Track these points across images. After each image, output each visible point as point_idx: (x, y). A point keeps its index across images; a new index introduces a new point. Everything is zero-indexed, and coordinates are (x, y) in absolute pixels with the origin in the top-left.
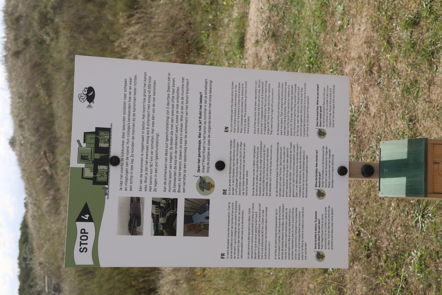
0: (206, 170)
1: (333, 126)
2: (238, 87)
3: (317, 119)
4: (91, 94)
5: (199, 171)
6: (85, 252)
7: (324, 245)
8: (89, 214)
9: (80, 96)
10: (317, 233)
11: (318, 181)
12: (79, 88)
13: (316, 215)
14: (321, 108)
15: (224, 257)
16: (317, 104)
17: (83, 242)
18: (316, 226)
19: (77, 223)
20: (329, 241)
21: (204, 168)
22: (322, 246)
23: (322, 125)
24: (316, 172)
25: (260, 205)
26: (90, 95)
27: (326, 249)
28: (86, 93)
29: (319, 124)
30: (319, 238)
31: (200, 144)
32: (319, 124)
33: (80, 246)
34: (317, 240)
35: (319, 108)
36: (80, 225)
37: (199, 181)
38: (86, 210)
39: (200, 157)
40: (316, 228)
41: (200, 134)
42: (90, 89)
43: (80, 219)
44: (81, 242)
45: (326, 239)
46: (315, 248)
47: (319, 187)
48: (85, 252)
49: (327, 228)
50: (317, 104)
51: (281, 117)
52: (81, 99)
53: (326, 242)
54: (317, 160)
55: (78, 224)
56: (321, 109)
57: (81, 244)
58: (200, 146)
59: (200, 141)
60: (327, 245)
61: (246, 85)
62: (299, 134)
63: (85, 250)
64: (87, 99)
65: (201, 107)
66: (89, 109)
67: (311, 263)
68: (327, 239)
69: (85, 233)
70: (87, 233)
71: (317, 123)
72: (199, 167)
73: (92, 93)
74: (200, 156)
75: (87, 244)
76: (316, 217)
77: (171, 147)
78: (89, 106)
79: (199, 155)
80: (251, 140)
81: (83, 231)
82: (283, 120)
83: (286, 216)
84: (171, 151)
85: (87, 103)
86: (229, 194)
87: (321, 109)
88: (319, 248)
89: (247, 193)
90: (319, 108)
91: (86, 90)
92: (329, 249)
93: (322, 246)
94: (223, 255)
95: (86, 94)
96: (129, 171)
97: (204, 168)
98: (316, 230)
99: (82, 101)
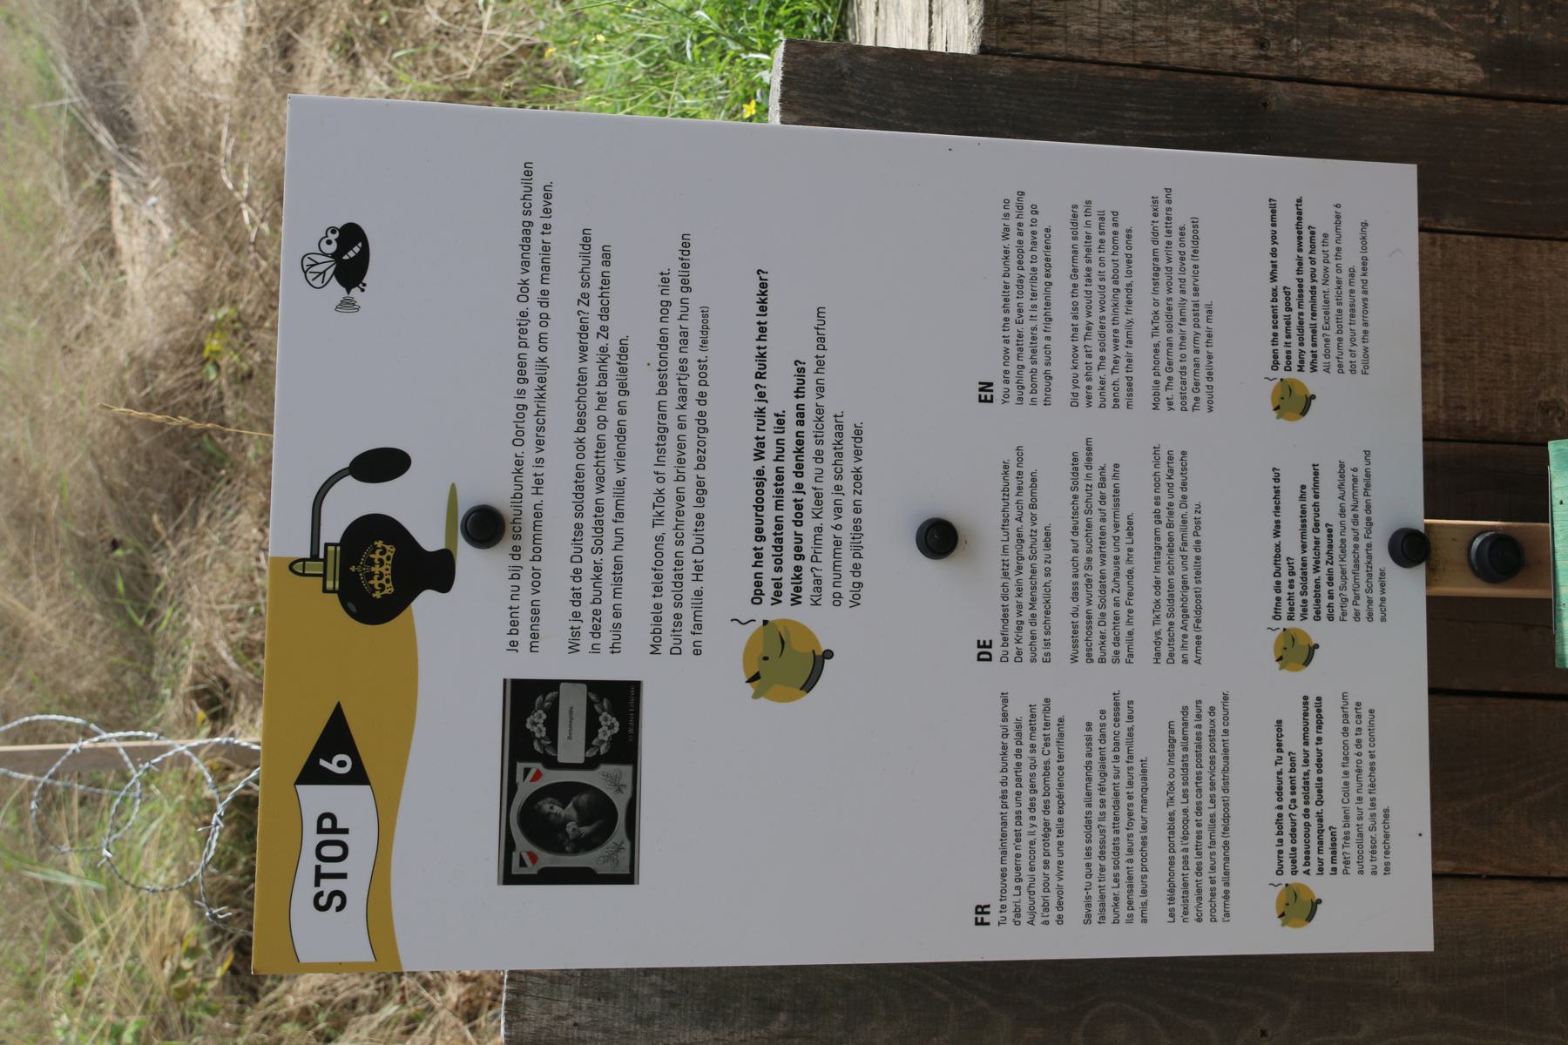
3: (1274, 342)
4: (351, 254)
6: (339, 909)
7: (1354, 859)
8: (353, 752)
9: (307, 262)
10: (1286, 811)
11: (1284, 596)
13: (1280, 736)
14: (1287, 294)
15: (987, 918)
16: (1273, 279)
17: (327, 868)
18: (1280, 781)
19: (303, 790)
20: (1373, 840)
22: (1347, 862)
24: (1277, 557)
25: (1005, 701)
27: (1361, 872)
28: (333, 248)
30: (1294, 830)
31: (760, 484)
32: (1282, 360)
33: (317, 884)
34: (1287, 838)
35: (1281, 296)
36: (316, 799)
38: (337, 735)
39: (763, 539)
40: (1280, 788)
41: (762, 445)
42: (351, 235)
43: (313, 774)
44: (318, 868)
45: (1361, 835)
46: (1280, 872)
47: (1290, 618)
48: (339, 909)
49: (1366, 788)
50: (1273, 279)
52: (310, 276)
53: (1360, 846)
54: (1277, 508)
56: (1288, 299)
57: (319, 876)
60: (1367, 856)
61: (1169, 202)
63: (337, 901)
66: (347, 317)
68: (1367, 835)
69: (334, 830)
70: (345, 831)
71: (1275, 357)
73: (356, 249)
75: (343, 876)
76: (1280, 745)
78: (347, 305)
79: (759, 530)
80: (1049, 433)
81: (327, 824)
85: (336, 290)
86: (1004, 658)
87: (1288, 299)
88: (1294, 872)
89: (1131, 655)
90: (1281, 296)
91: (333, 237)
92: (1374, 873)
93: (1347, 862)
94: (981, 910)
95: (333, 255)
96: (1192, 583)
98: (1280, 799)
99: (318, 283)
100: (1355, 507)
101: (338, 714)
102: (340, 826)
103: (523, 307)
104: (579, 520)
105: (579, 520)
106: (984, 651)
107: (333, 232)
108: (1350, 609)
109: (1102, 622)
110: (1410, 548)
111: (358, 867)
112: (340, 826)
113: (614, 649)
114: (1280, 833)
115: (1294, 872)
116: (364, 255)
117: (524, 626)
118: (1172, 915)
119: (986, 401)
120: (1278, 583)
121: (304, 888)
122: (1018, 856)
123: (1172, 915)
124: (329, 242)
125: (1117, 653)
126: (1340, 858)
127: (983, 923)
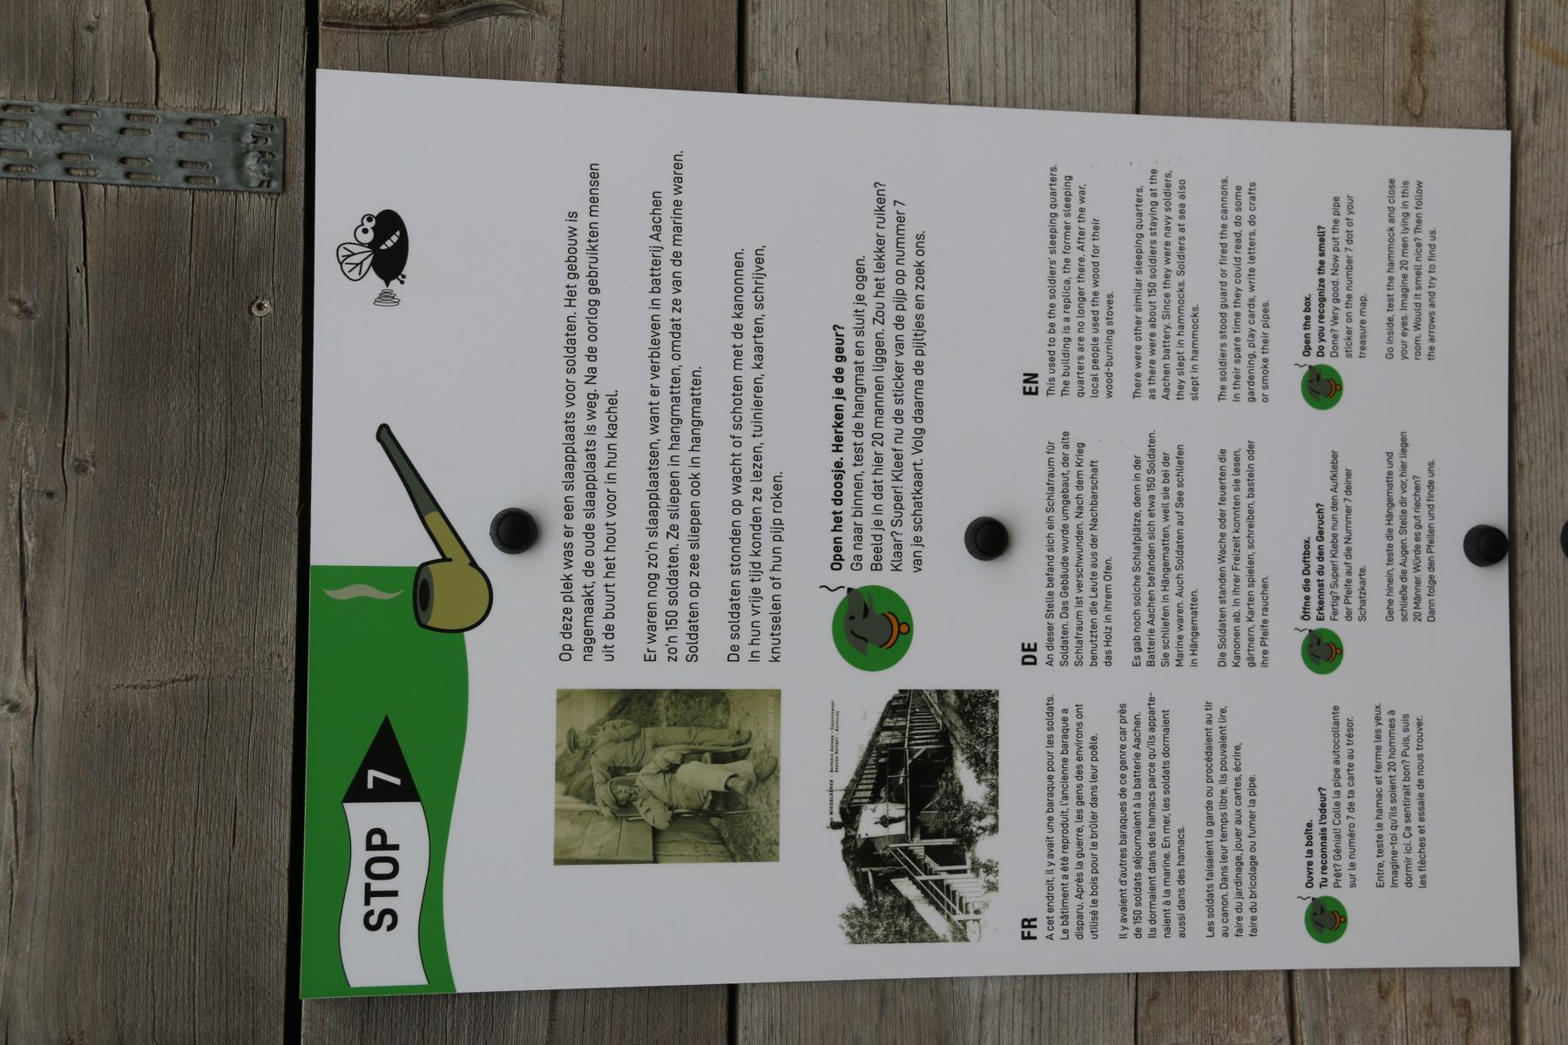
1: (1431, 357)
3: (1306, 326)
4: (389, 243)
6: (390, 928)
9: (343, 252)
12: (338, 223)
15: (1033, 932)
17: (377, 886)
19: (346, 805)
21: (898, 554)
23: (1315, 349)
26: (388, 245)
28: (369, 237)
29: (1315, 345)
31: (839, 477)
33: (367, 903)
36: (362, 817)
38: (385, 750)
39: (844, 359)
42: (388, 223)
43: (357, 793)
44: (368, 886)
46: (1309, 884)
48: (390, 928)
52: (347, 268)
55: (352, 809)
57: (369, 894)
58: (838, 486)
59: (838, 464)
63: (388, 920)
64: (372, 264)
65: (838, 520)
67: (1284, 945)
70: (396, 847)
72: (838, 549)
73: (395, 238)
74: (840, 357)
75: (394, 894)
77: (674, 528)
78: (386, 298)
79: (839, 350)
80: (1114, 428)
81: (376, 840)
85: (374, 282)
91: (369, 225)
93: (1338, 875)
94: (1028, 923)
95: (370, 245)
97: (898, 554)
99: (355, 274)
102: (389, 842)
104: (918, 533)
105: (918, 533)
107: (370, 220)
108: (1342, 608)
109: (671, 622)
110: (1486, 546)
112: (389, 842)
113: (693, 657)
114: (1309, 843)
116: (403, 245)
117: (584, 631)
118: (1211, 929)
119: (1030, 393)
120: (1307, 581)
123: (1211, 929)
124: (365, 231)
125: (1166, 655)
126: (1330, 871)
127: (1029, 937)
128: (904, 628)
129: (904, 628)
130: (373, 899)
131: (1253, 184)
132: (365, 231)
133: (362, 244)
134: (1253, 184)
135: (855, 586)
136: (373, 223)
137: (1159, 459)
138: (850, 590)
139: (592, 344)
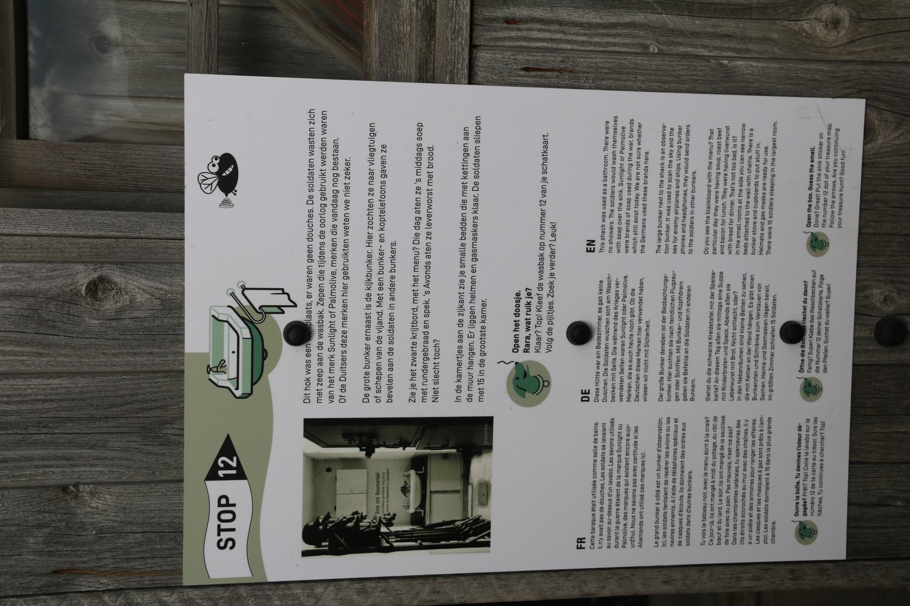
0: (544, 346)
2: (627, 130)
4: (228, 172)
5: (516, 349)
6: (231, 548)
9: (201, 178)
12: (197, 160)
15: (583, 545)
17: (224, 526)
20: (815, 441)
21: (539, 343)
26: (227, 175)
28: (216, 169)
31: (518, 301)
33: (219, 535)
36: (216, 488)
37: (514, 373)
38: (228, 449)
42: (227, 160)
43: (213, 475)
44: (219, 526)
46: (797, 514)
47: (526, 351)
48: (231, 548)
51: (611, 220)
57: (220, 530)
58: (518, 306)
62: (742, 249)
63: (230, 544)
66: (226, 211)
69: (228, 505)
70: (234, 505)
73: (230, 169)
75: (234, 530)
78: (226, 203)
80: (647, 268)
81: (223, 501)
82: (616, 226)
83: (675, 439)
84: (320, 308)
85: (219, 195)
88: (805, 515)
91: (216, 162)
95: (217, 173)
97: (539, 343)
99: (208, 190)
100: (623, 337)
101: (228, 437)
102: (230, 502)
103: (310, 207)
106: (585, 396)
107: (216, 159)
111: (242, 525)
112: (230, 502)
115: (805, 515)
116: (235, 172)
119: (590, 251)
121: (212, 537)
122: (618, 509)
124: (214, 165)
127: (581, 548)
128: (546, 384)
129: (546, 384)
130: (222, 533)
131: (688, 126)
132: (214, 165)
133: (212, 173)
134: (688, 126)
135: (519, 361)
136: (218, 161)
137: (629, 291)
138: (516, 363)
139: (323, 229)
